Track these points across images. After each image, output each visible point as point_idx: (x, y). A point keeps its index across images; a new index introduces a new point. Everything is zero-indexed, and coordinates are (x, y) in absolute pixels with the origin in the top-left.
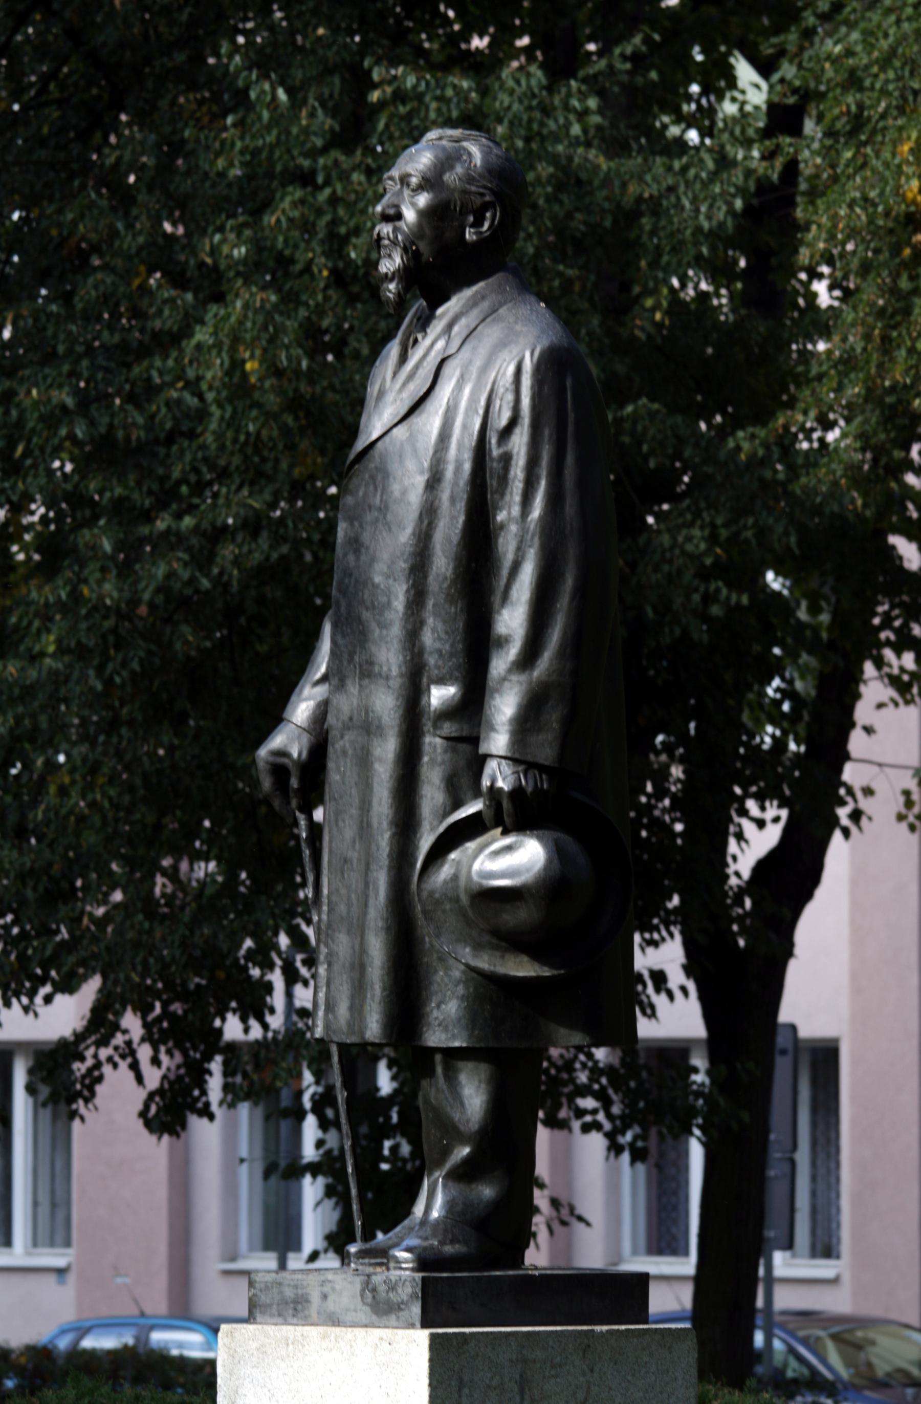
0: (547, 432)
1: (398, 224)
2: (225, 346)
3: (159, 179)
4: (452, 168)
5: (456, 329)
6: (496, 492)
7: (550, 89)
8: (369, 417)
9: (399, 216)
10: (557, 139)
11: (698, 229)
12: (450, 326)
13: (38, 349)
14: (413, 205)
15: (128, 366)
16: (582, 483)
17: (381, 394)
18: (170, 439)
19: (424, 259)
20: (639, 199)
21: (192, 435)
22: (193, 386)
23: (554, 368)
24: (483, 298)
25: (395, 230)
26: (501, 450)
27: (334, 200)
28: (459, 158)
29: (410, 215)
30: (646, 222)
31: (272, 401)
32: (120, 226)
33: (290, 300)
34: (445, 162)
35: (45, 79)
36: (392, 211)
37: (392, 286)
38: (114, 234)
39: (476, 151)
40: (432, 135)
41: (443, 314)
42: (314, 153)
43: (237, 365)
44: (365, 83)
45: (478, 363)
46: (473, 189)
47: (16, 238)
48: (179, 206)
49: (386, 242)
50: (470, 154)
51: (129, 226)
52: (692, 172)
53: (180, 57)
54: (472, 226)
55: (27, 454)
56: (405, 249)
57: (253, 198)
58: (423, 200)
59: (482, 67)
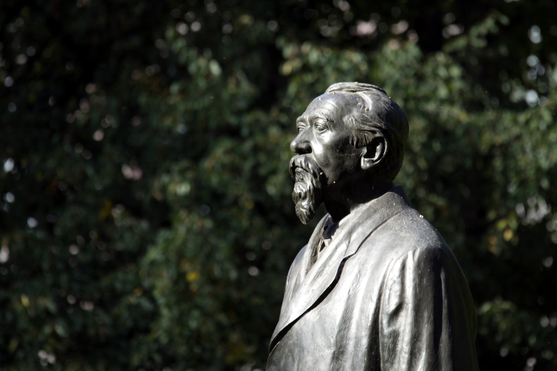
0: (426, 314)
1: (308, 155)
2: (169, 267)
3: (117, 137)
4: (350, 111)
5: (354, 236)
6: (387, 361)
7: (423, 61)
8: (288, 305)
9: (309, 150)
10: (427, 99)
11: (539, 169)
12: (350, 234)
13: (25, 266)
14: (320, 140)
15: (96, 278)
16: (453, 355)
17: (297, 287)
18: (132, 333)
19: (329, 182)
20: (493, 147)
21: (147, 331)
22: (148, 293)
23: (433, 264)
24: (375, 211)
25: (307, 160)
26: (391, 329)
27: (256, 149)
28: (355, 105)
29: (318, 149)
30: (498, 163)
31: (209, 303)
32: (90, 171)
33: (222, 226)
34: (346, 106)
35: (31, 61)
36: (303, 146)
37: (305, 203)
38: (85, 177)
39: (369, 99)
40: (334, 87)
41: (345, 224)
42: (239, 113)
43: (181, 276)
44: (278, 58)
45: (372, 261)
46: (367, 128)
47: (9, 182)
48: (137, 156)
49: (300, 169)
50: (363, 101)
51: (98, 171)
52: (533, 125)
53: (136, 41)
54: (366, 157)
55: (20, 347)
56: (315, 175)
57: (193, 149)
58: (328, 136)
59: (370, 46)
